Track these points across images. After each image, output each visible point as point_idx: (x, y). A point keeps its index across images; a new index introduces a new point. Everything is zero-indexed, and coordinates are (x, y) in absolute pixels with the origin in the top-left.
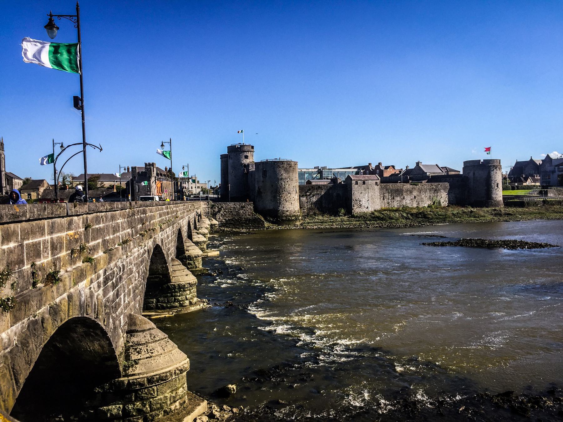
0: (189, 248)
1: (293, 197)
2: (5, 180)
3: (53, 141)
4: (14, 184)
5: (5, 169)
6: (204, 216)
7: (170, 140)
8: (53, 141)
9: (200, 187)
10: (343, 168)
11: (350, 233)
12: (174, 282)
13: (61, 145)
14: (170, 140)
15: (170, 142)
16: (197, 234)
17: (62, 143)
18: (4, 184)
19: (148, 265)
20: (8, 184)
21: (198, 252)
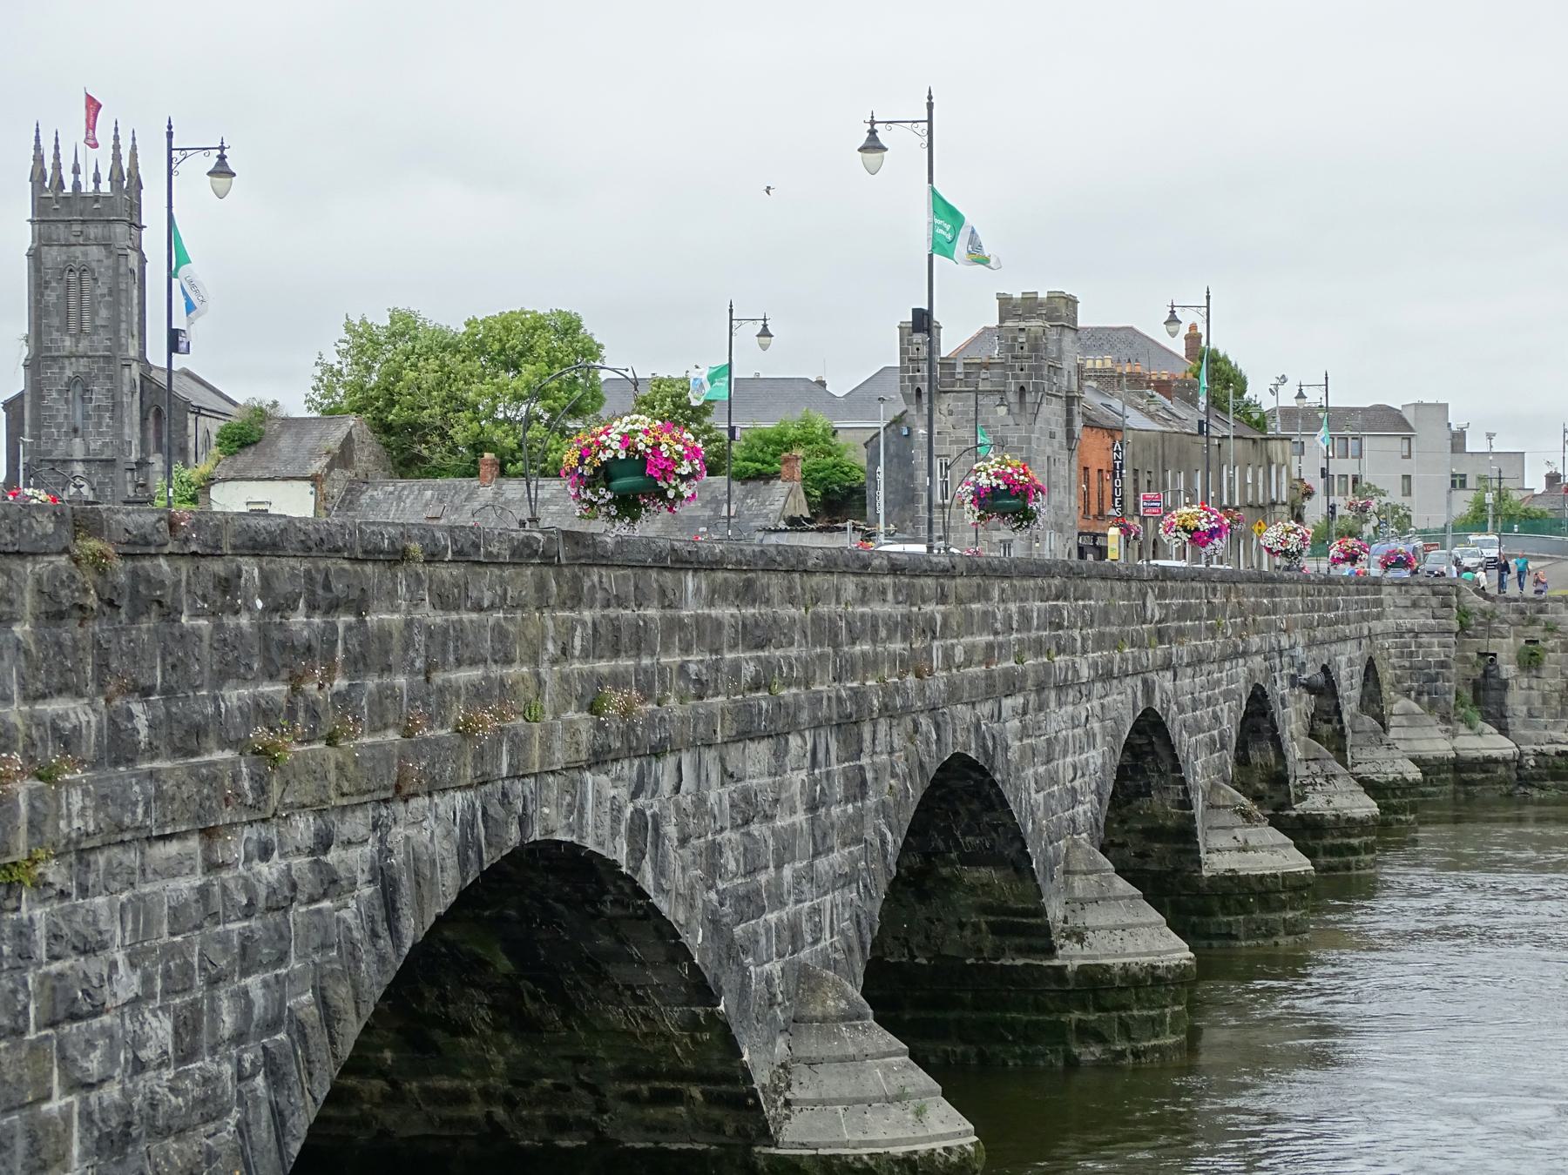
0: (1093, 917)
1: (515, 526)
2: (144, 420)
3: (170, 135)
4: (191, 445)
5: (143, 345)
6: (1406, 693)
7: (930, 106)
8: (170, 135)
9: (1471, 482)
10: (57, 147)
11: (864, 922)
12: (792, 1145)
13: (213, 160)
14: (930, 106)
15: (930, 121)
16: (1239, 820)
17: (222, 148)
18: (136, 442)
19: (863, 1006)
20: (159, 449)
21: (1161, 946)
